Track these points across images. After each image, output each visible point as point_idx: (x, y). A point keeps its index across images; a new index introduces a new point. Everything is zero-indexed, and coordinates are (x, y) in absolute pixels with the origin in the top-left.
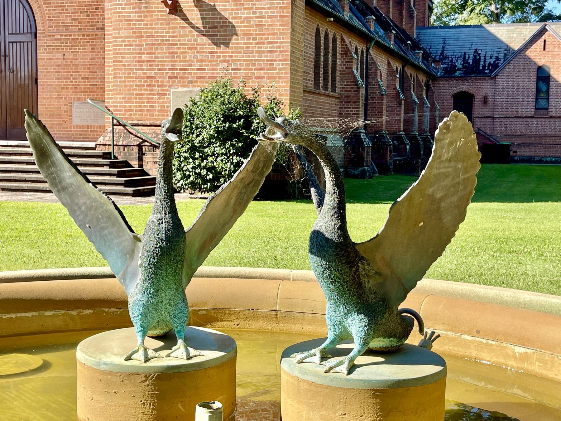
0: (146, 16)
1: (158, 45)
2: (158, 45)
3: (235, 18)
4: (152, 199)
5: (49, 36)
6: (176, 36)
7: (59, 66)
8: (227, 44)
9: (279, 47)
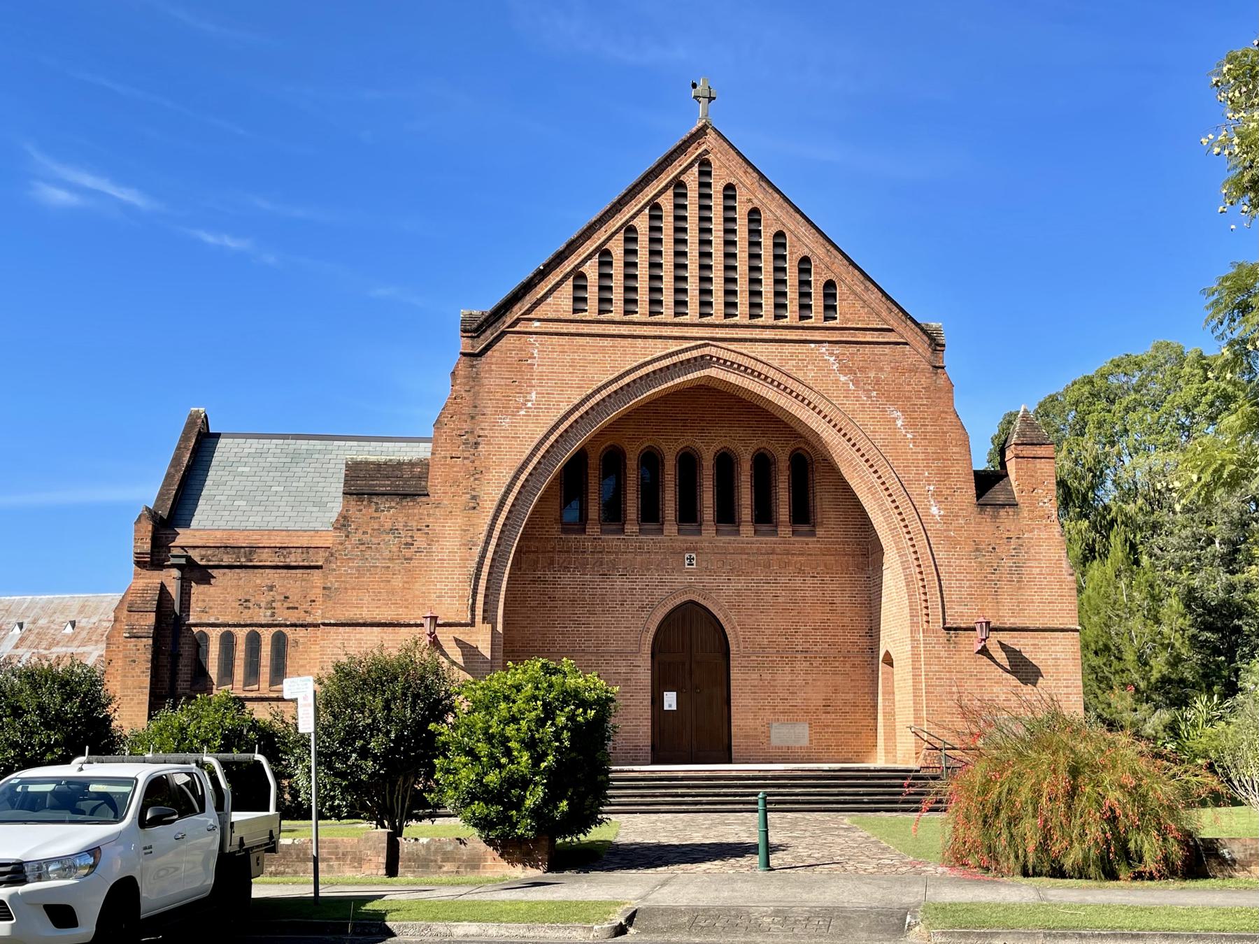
0: (955, 654)
1: (967, 679)
2: (967, 679)
3: (1034, 659)
4: (757, 814)
5: (744, 657)
6: (983, 672)
7: (755, 686)
8: (1034, 684)
9: (1073, 683)
